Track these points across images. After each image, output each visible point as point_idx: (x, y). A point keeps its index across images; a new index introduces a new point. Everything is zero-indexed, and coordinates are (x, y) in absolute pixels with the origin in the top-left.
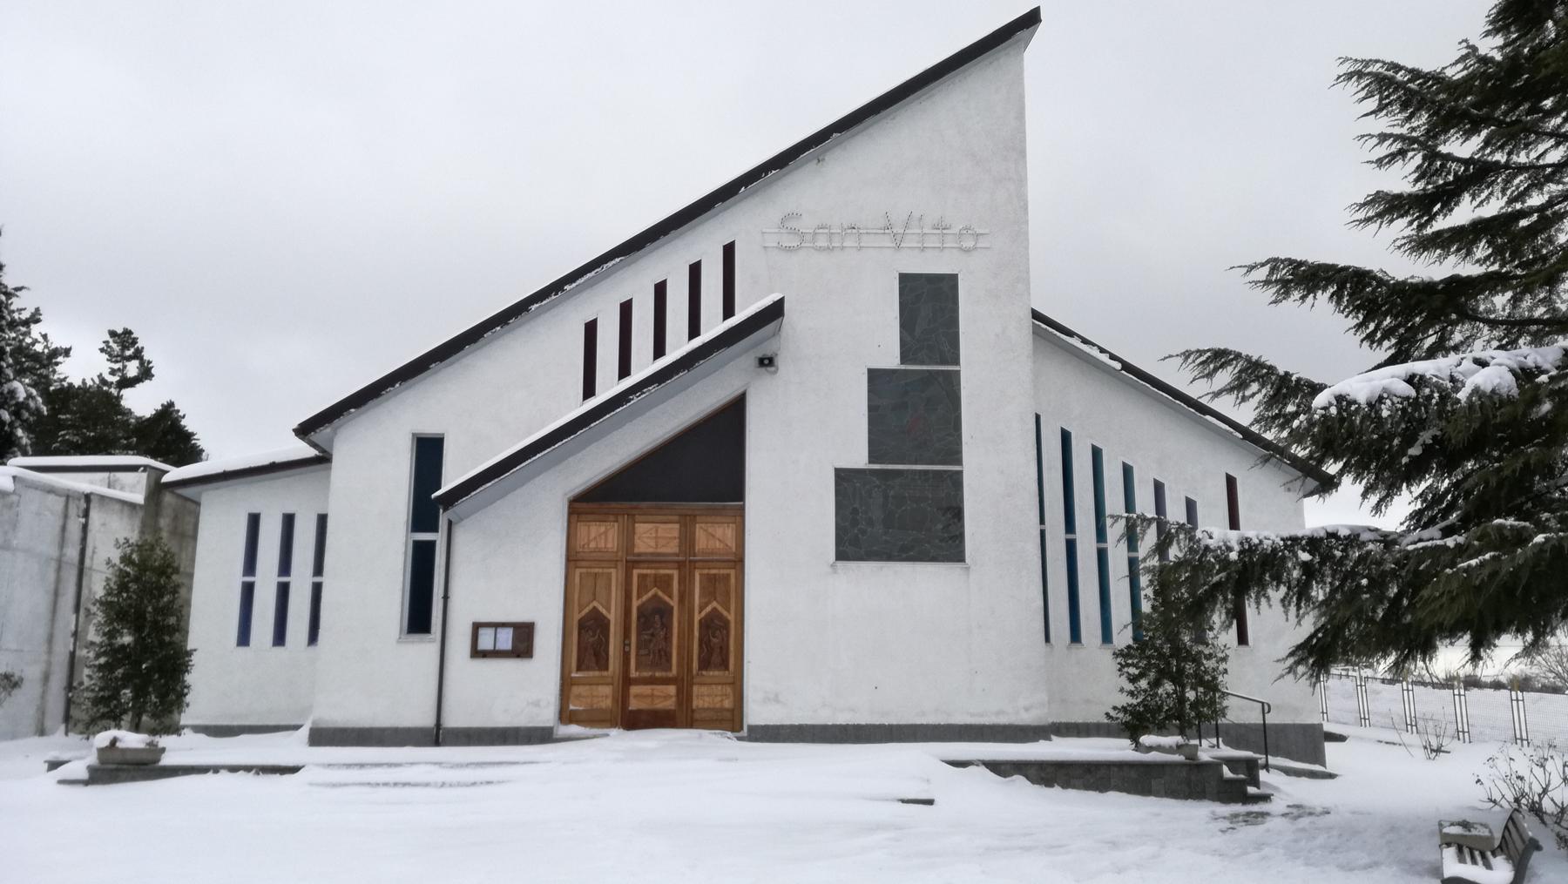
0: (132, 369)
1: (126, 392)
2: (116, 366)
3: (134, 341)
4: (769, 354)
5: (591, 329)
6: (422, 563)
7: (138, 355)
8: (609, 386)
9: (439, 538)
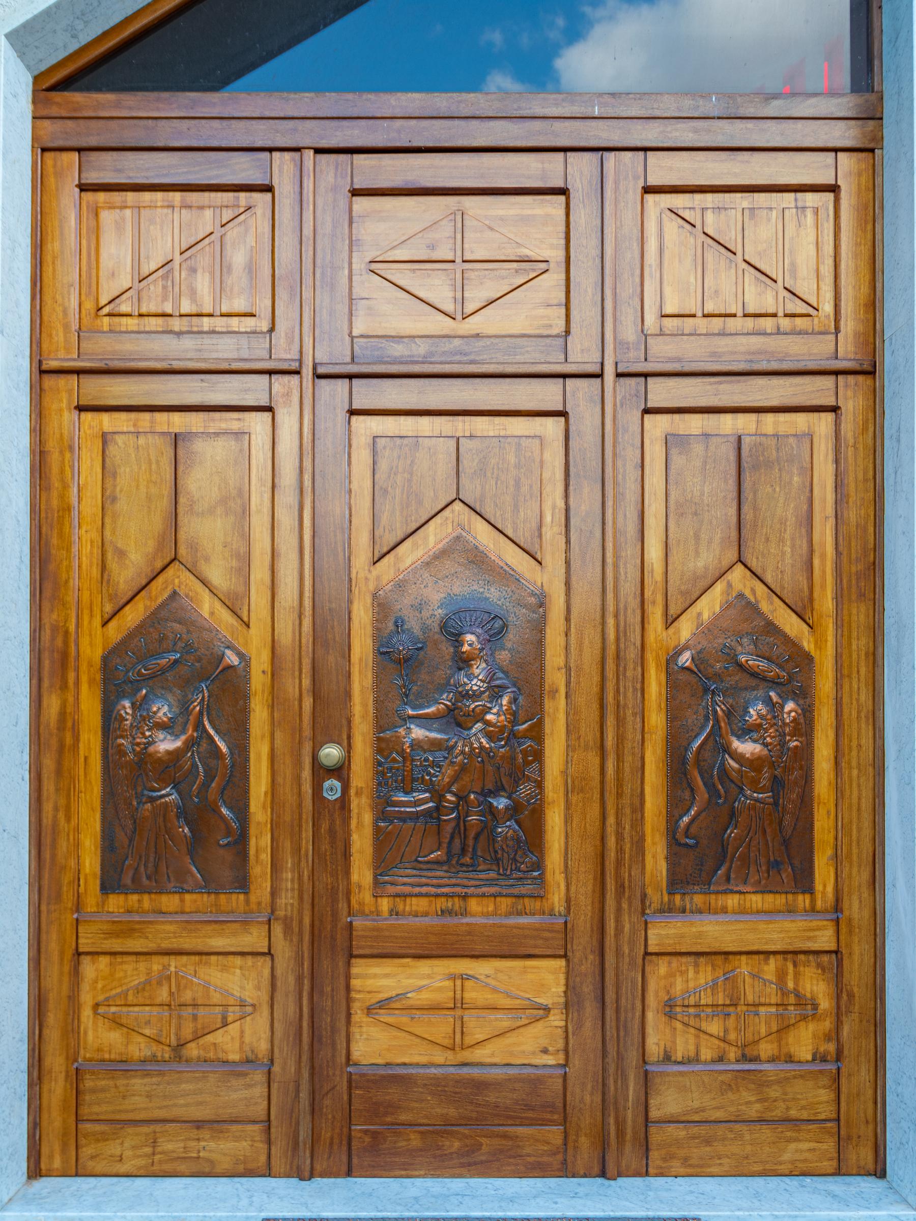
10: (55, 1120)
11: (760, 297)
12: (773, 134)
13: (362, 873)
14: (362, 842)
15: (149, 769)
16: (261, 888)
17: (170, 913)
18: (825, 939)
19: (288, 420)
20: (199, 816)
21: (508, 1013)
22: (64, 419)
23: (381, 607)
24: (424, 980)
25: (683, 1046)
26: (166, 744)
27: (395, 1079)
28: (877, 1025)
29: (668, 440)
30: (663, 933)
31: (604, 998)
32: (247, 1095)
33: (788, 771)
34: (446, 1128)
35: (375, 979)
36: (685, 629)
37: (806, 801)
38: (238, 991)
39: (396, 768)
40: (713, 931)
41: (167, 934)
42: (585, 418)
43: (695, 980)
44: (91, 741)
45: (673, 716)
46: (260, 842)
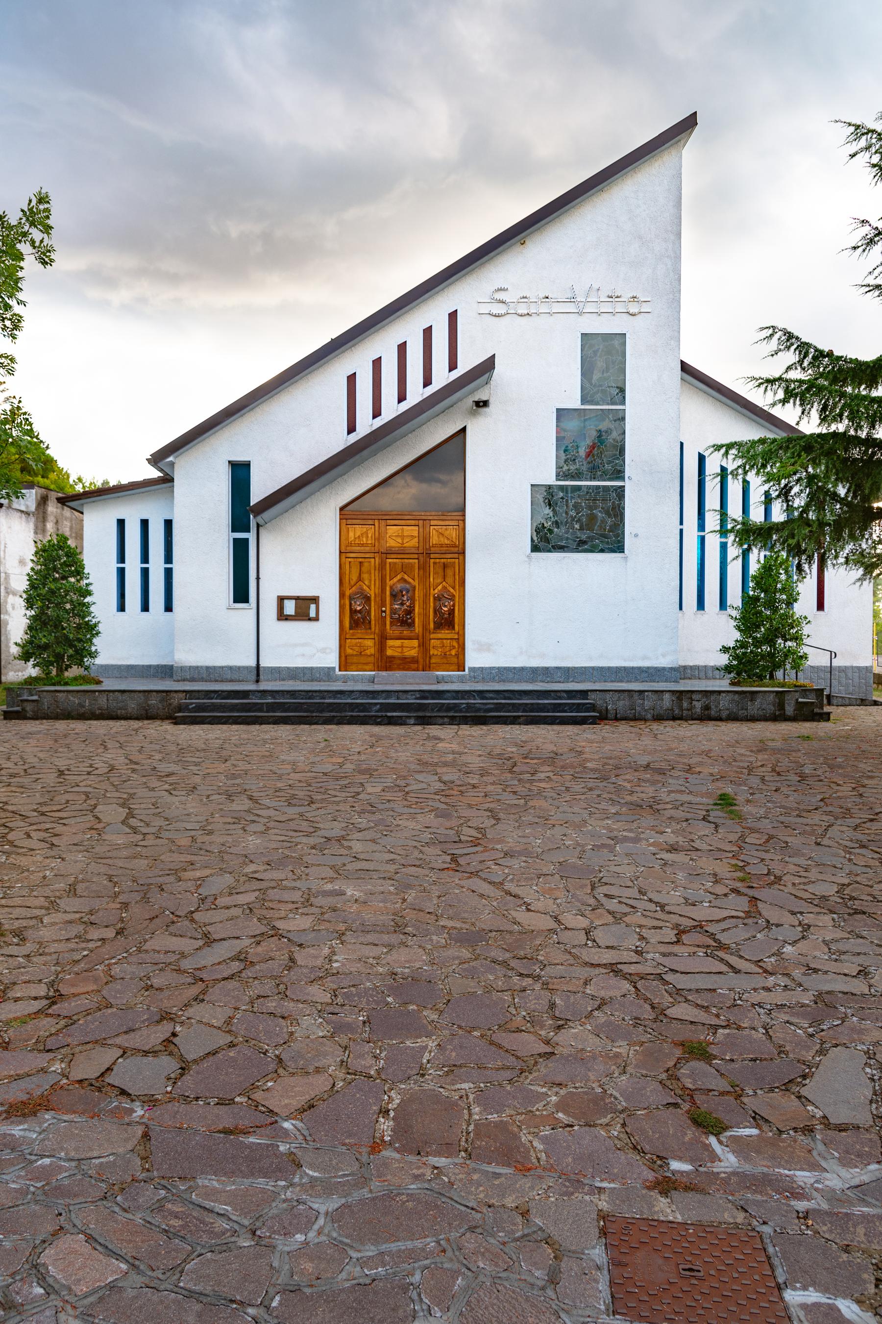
4: (485, 399)
5: (352, 379)
6: (240, 550)
8: (366, 424)
9: (251, 536)
10: (343, 663)
11: (446, 542)
12: (449, 518)
13: (388, 627)
14: (388, 623)
15: (356, 611)
16: (373, 629)
17: (360, 632)
18: (456, 637)
19: (377, 559)
20: (364, 618)
21: (411, 648)
22: (343, 559)
23: (391, 587)
24: (398, 643)
25: (436, 653)
26: (359, 608)
27: (393, 657)
28: (464, 649)
29: (434, 563)
30: (432, 636)
31: (424, 646)
32: (371, 659)
33: (452, 612)
34: (400, 664)
35: (390, 643)
36: (436, 591)
37: (454, 616)
38: (370, 645)
39: (394, 612)
40: (440, 636)
41: (359, 636)
42: (421, 559)
43: (438, 643)
44: (348, 607)
45: (434, 604)
46: (373, 622)
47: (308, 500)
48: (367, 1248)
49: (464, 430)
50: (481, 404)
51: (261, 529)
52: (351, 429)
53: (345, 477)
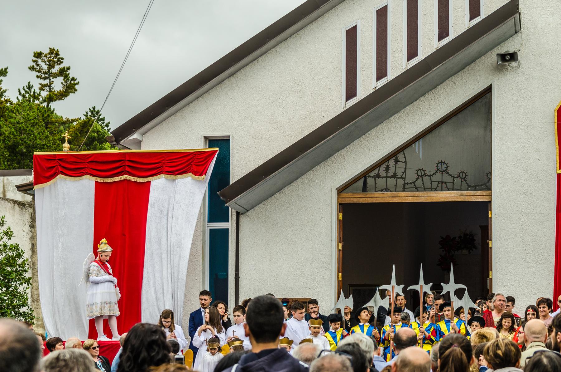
0: (58, 85)
1: (53, 105)
2: (47, 82)
3: (60, 61)
4: (512, 51)
5: (351, 35)
6: (218, 244)
7: (63, 72)
8: (367, 84)
9: (230, 225)
47: (299, 181)
48: (128, 353)
49: (489, 90)
50: (508, 57)
51: (242, 219)
52: (351, 92)
53: (343, 151)
